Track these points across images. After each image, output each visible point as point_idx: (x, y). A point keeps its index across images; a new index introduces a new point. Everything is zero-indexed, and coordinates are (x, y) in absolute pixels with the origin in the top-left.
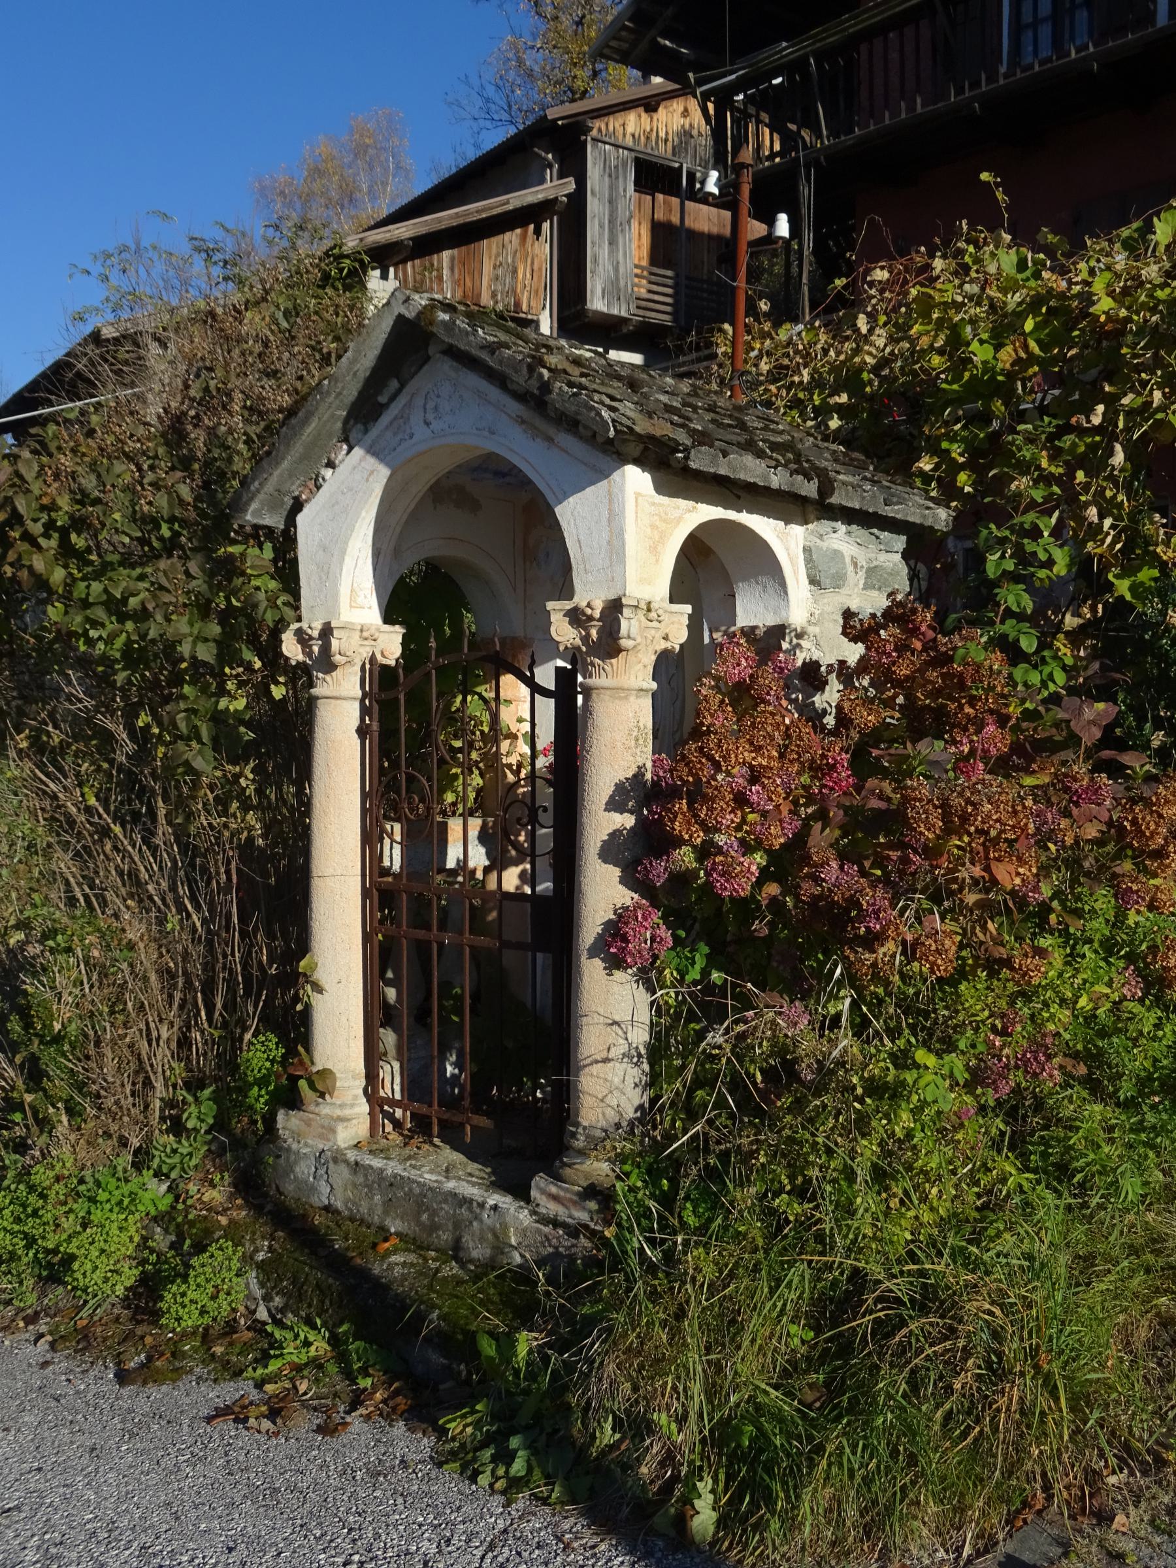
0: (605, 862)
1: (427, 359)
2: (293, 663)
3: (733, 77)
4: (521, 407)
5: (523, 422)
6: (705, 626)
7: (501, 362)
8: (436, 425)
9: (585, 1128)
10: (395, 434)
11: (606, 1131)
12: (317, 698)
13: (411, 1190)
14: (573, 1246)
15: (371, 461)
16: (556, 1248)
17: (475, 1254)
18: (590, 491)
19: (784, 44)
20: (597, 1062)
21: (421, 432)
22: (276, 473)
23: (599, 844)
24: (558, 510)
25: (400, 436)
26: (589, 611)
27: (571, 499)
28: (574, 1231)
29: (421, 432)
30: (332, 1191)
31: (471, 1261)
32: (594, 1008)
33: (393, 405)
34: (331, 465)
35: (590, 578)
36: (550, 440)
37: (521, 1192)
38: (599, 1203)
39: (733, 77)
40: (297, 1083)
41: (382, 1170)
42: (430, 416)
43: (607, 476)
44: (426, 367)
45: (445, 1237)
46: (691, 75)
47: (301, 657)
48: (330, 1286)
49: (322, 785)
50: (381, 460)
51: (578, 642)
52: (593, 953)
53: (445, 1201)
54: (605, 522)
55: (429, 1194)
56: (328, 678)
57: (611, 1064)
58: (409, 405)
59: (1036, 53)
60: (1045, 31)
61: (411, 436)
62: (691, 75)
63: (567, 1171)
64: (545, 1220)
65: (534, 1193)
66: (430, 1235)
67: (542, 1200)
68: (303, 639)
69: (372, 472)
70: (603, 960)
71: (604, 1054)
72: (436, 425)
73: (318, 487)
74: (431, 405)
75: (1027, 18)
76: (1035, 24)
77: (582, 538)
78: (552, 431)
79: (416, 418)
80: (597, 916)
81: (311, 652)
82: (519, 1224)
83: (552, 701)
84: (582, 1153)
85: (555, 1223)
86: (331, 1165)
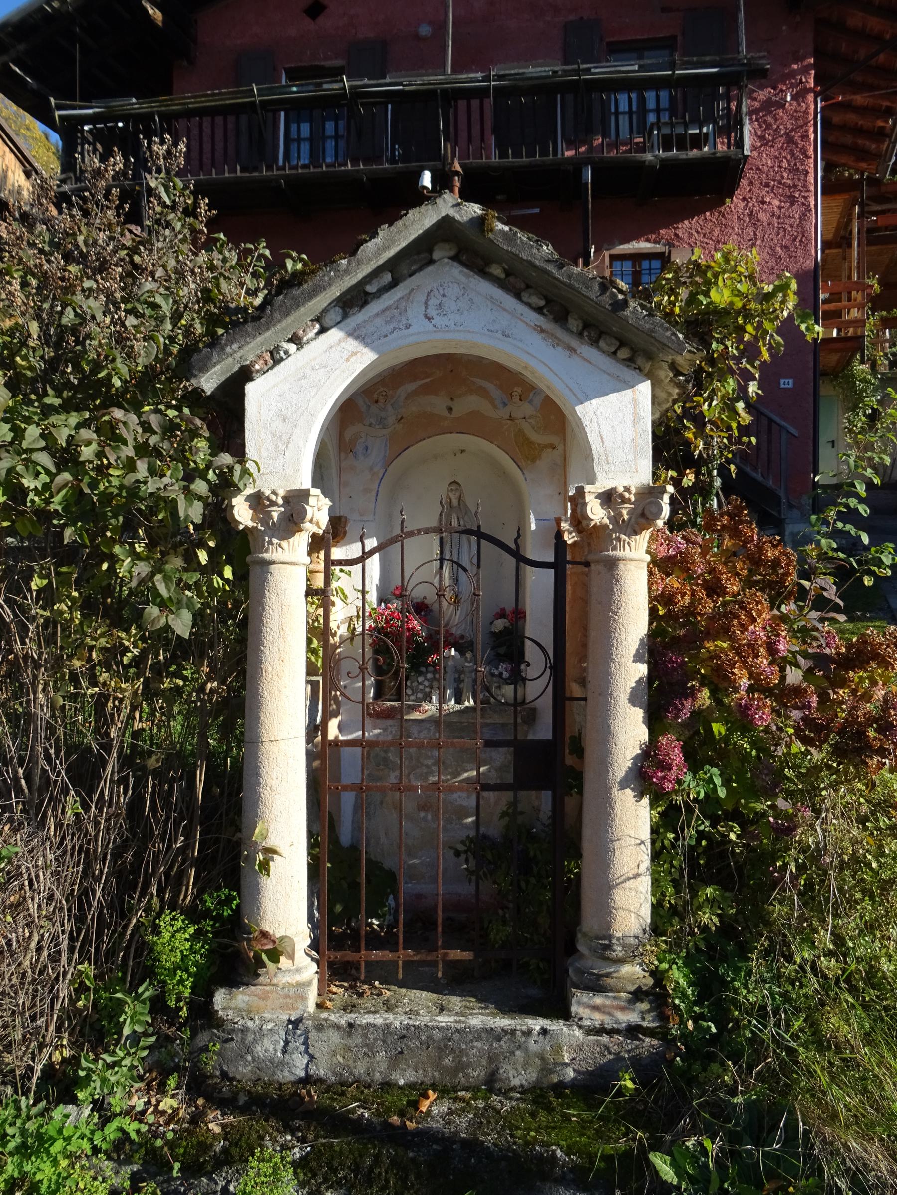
0: (634, 705)
1: (431, 262)
2: (241, 527)
3: (90, 111)
4: (542, 318)
5: (542, 331)
6: (532, 516)
7: (570, 277)
8: (437, 320)
9: (618, 939)
10: (387, 323)
11: (637, 938)
12: (619, 560)
13: (429, 1037)
14: (637, 1047)
15: (352, 344)
16: (617, 1054)
17: (516, 1082)
18: (613, 397)
19: (134, 100)
20: (629, 879)
21: (419, 325)
22: (260, 339)
23: (629, 691)
24: (579, 409)
25: (394, 325)
26: (273, 497)
27: (593, 401)
28: (633, 1031)
29: (419, 325)
30: (326, 1057)
31: (513, 1089)
32: (626, 832)
33: (386, 296)
34: (295, 339)
35: (612, 467)
36: (572, 350)
37: (562, 1012)
38: (650, 1002)
39: (90, 111)
40: (235, 954)
41: (388, 1026)
42: (432, 312)
43: (633, 386)
44: (431, 268)
45: (477, 1074)
46: (52, 99)
47: (250, 524)
48: (413, 1160)
49: (274, 649)
50: (367, 345)
51: (606, 521)
52: (623, 785)
53: (479, 1038)
54: (629, 423)
55: (456, 1036)
56: (284, 544)
57: (639, 879)
58: (407, 298)
59: (299, 158)
60: (305, 148)
61: (408, 327)
62: (52, 99)
63: (609, 981)
64: (590, 1031)
65: (574, 1009)
66: (456, 1076)
67: (584, 1012)
68: (258, 501)
69: (356, 353)
70: (633, 790)
71: (635, 871)
72: (437, 320)
73: (277, 361)
74: (433, 302)
75: (294, 135)
76: (299, 140)
77: (604, 434)
78: (574, 343)
79: (415, 312)
80: (628, 752)
81: (268, 515)
82: (574, 1039)
83: (552, 571)
84: (622, 961)
85: (601, 1031)
86: (313, 1034)
